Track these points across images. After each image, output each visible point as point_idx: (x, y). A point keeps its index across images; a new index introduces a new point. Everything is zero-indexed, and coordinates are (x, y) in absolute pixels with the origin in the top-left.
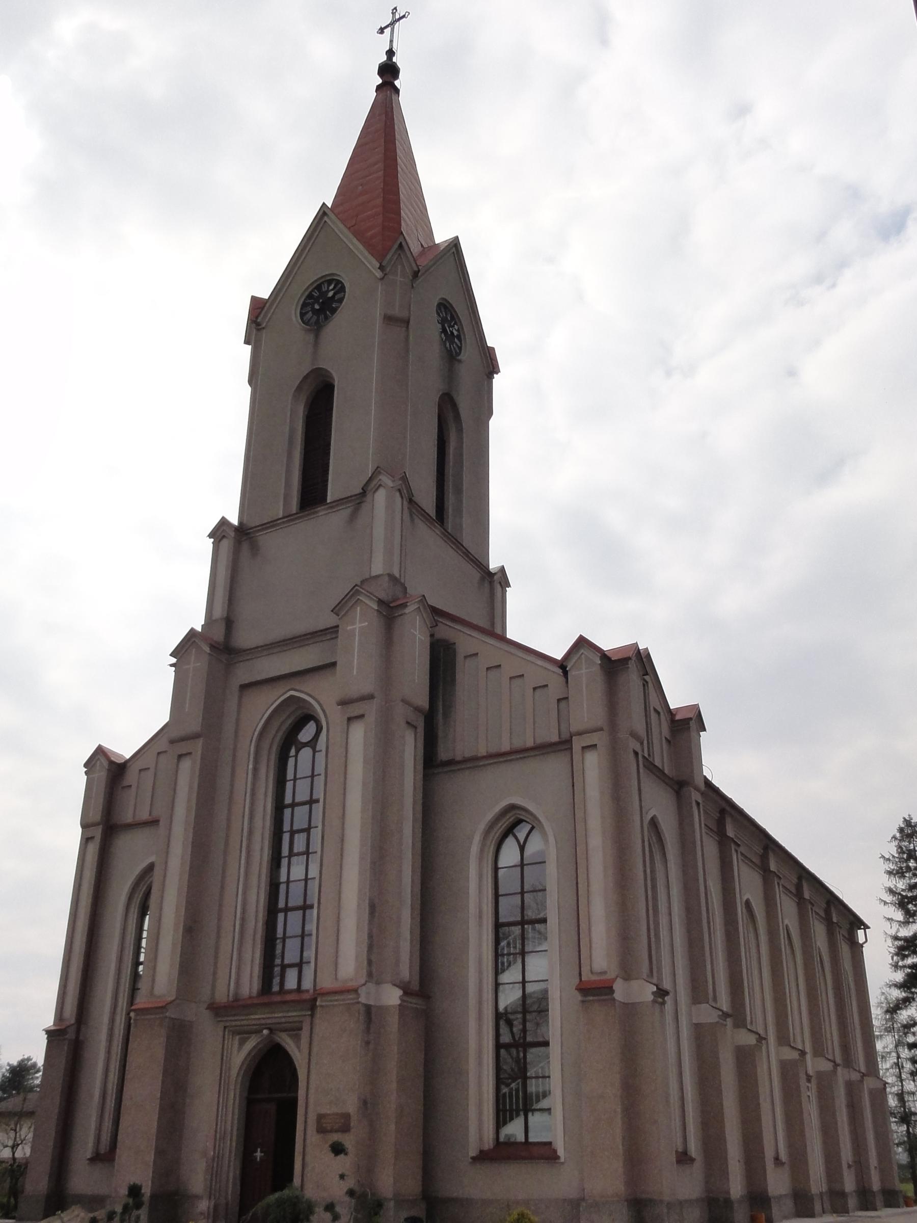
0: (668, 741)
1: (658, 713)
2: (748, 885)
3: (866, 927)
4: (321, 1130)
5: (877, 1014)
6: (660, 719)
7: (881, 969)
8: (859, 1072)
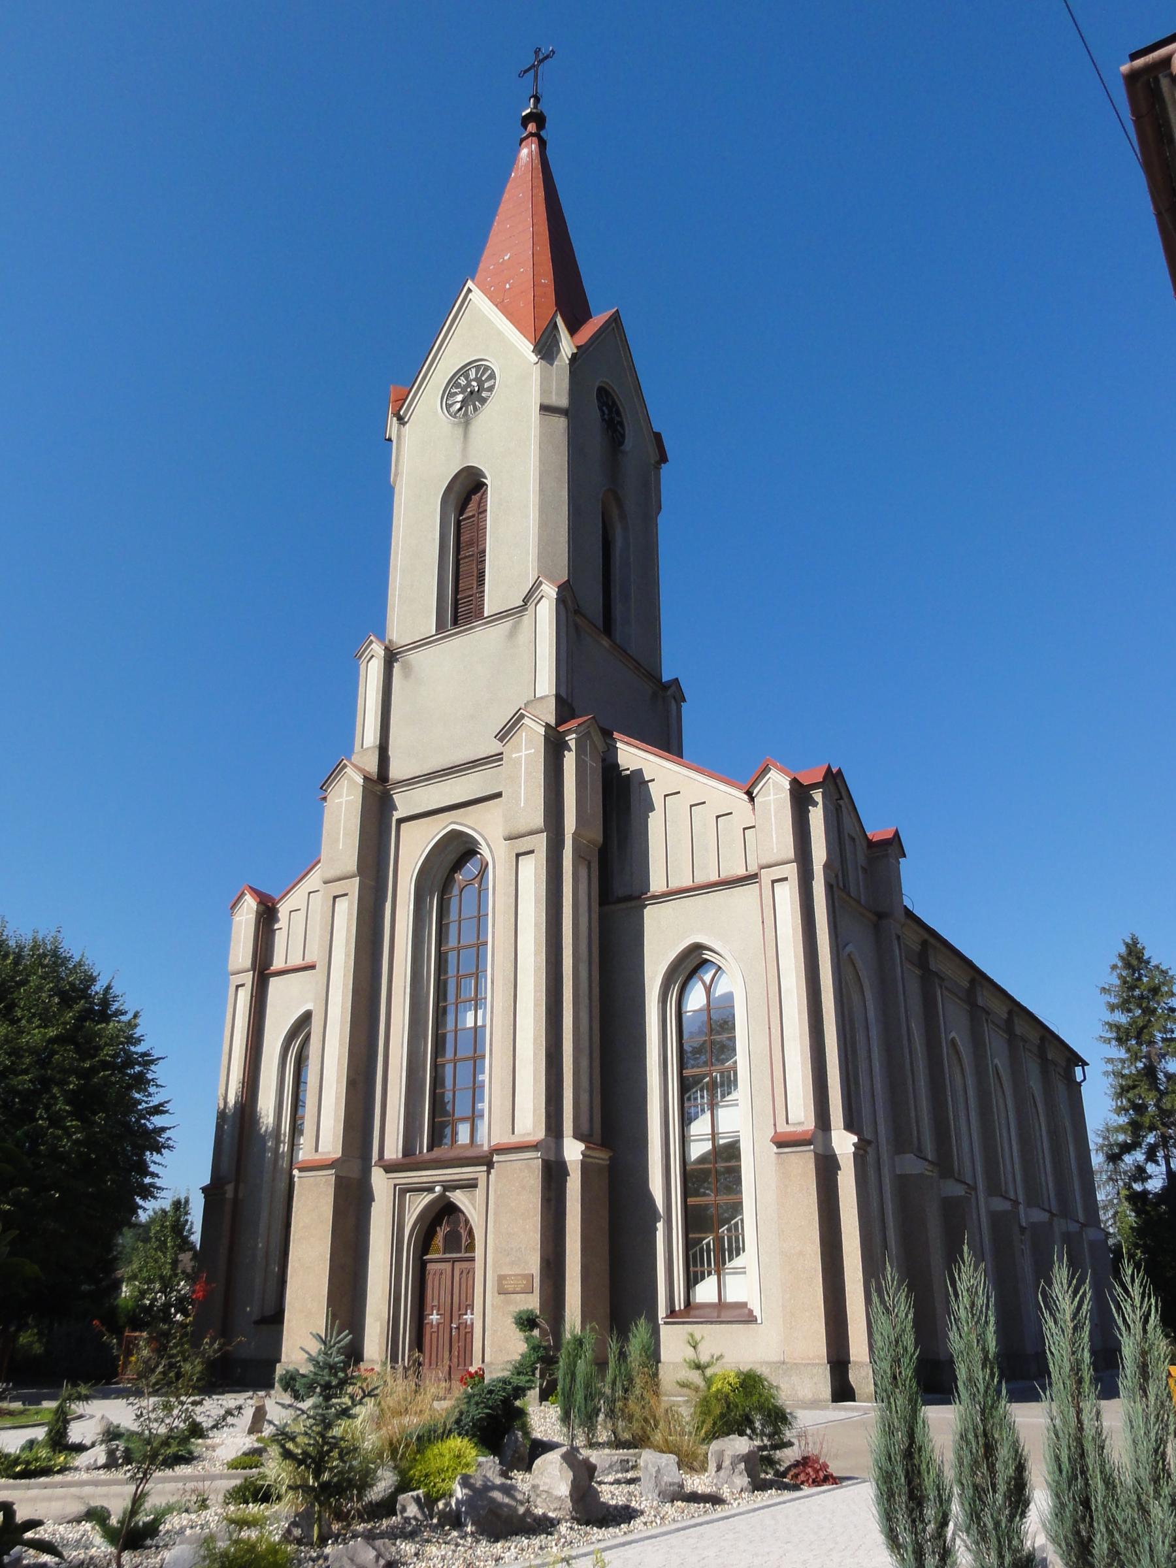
0: (864, 870)
1: (853, 839)
2: (955, 1027)
3: (1085, 1064)
4: (502, 1291)
5: (1097, 1159)
6: (855, 846)
7: (1101, 1110)
8: (1078, 1222)
